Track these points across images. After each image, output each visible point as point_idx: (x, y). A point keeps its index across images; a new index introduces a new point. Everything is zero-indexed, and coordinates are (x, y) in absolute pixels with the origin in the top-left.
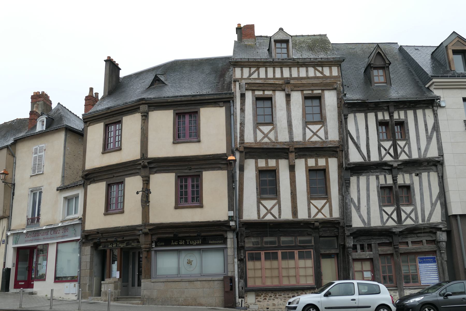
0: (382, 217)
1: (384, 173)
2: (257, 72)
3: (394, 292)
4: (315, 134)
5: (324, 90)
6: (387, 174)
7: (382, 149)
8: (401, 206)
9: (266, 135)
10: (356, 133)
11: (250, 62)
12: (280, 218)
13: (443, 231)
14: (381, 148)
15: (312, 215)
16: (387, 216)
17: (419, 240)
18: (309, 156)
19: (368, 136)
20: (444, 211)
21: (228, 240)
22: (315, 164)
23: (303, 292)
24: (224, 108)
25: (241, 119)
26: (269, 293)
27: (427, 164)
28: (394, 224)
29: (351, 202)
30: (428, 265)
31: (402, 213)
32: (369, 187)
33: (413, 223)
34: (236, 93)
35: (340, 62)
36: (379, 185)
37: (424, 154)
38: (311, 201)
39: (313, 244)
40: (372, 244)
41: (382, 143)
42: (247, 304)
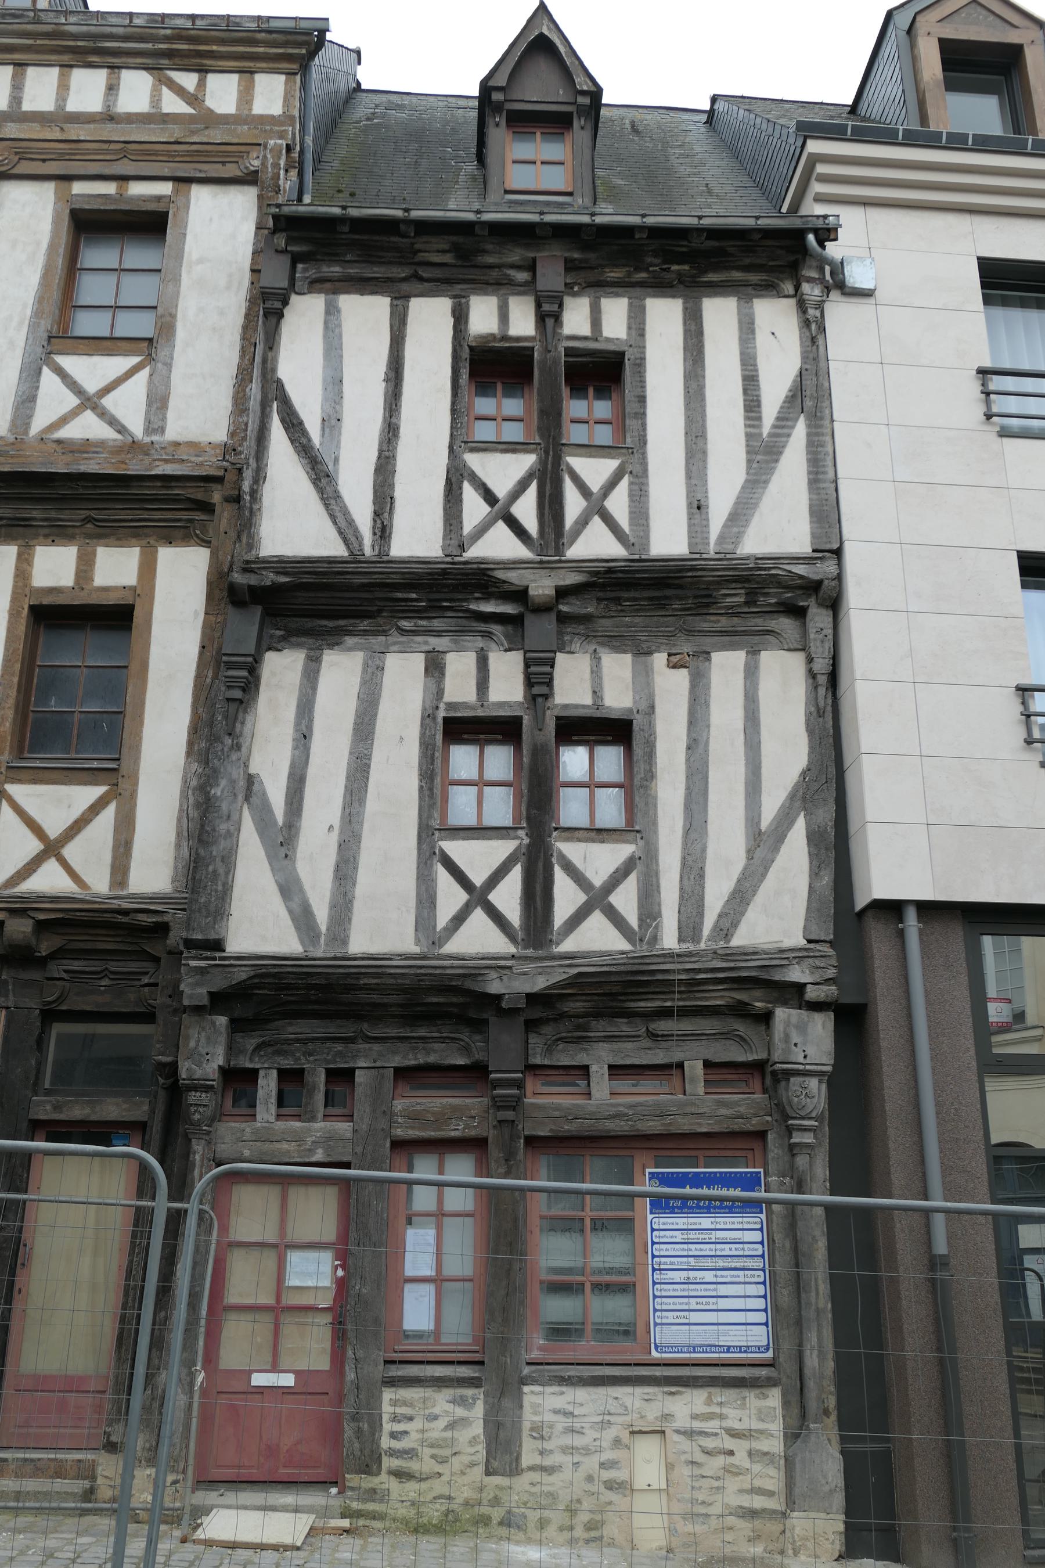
0: (426, 899)
1: (480, 642)
3: (453, 1402)
4: (90, 402)
5: (189, 180)
6: (499, 644)
7: (470, 495)
8: (555, 834)
10: (325, 399)
13: (816, 1006)
14: (466, 486)
16: (462, 896)
17: (659, 1057)
18: (46, 531)
19: (394, 420)
20: (827, 879)
27: (747, 603)
28: (497, 943)
29: (241, 797)
30: (706, 1222)
31: (560, 877)
33: (623, 945)
36: (437, 708)
37: (722, 538)
40: (357, 1072)
41: (474, 461)
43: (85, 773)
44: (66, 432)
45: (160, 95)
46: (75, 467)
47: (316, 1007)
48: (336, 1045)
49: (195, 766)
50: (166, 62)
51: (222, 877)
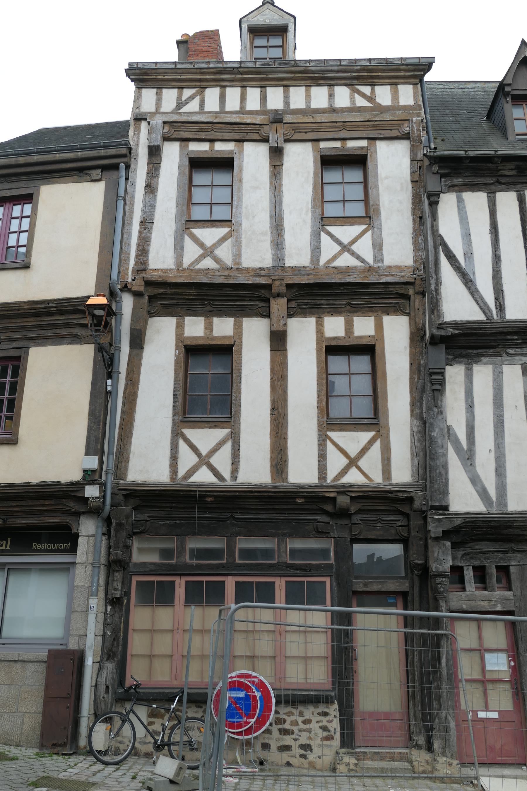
2: (198, 98)
4: (346, 248)
5: (375, 139)
9: (209, 250)
10: (464, 244)
11: (179, 71)
12: (236, 480)
15: (331, 474)
18: (328, 310)
19: (497, 253)
21: (80, 540)
22: (345, 330)
23: (294, 711)
24: (102, 185)
25: (144, 211)
26: (191, 707)
29: (446, 437)
32: (502, 395)
34: (137, 148)
35: (420, 70)
38: (331, 434)
39: (332, 561)
40: (511, 567)
42: (119, 739)
43: (363, 426)
44: (337, 263)
45: (354, 98)
46: (344, 280)
47: (490, 536)
48: (499, 554)
49: (415, 422)
50: (356, 81)
51: (444, 475)
